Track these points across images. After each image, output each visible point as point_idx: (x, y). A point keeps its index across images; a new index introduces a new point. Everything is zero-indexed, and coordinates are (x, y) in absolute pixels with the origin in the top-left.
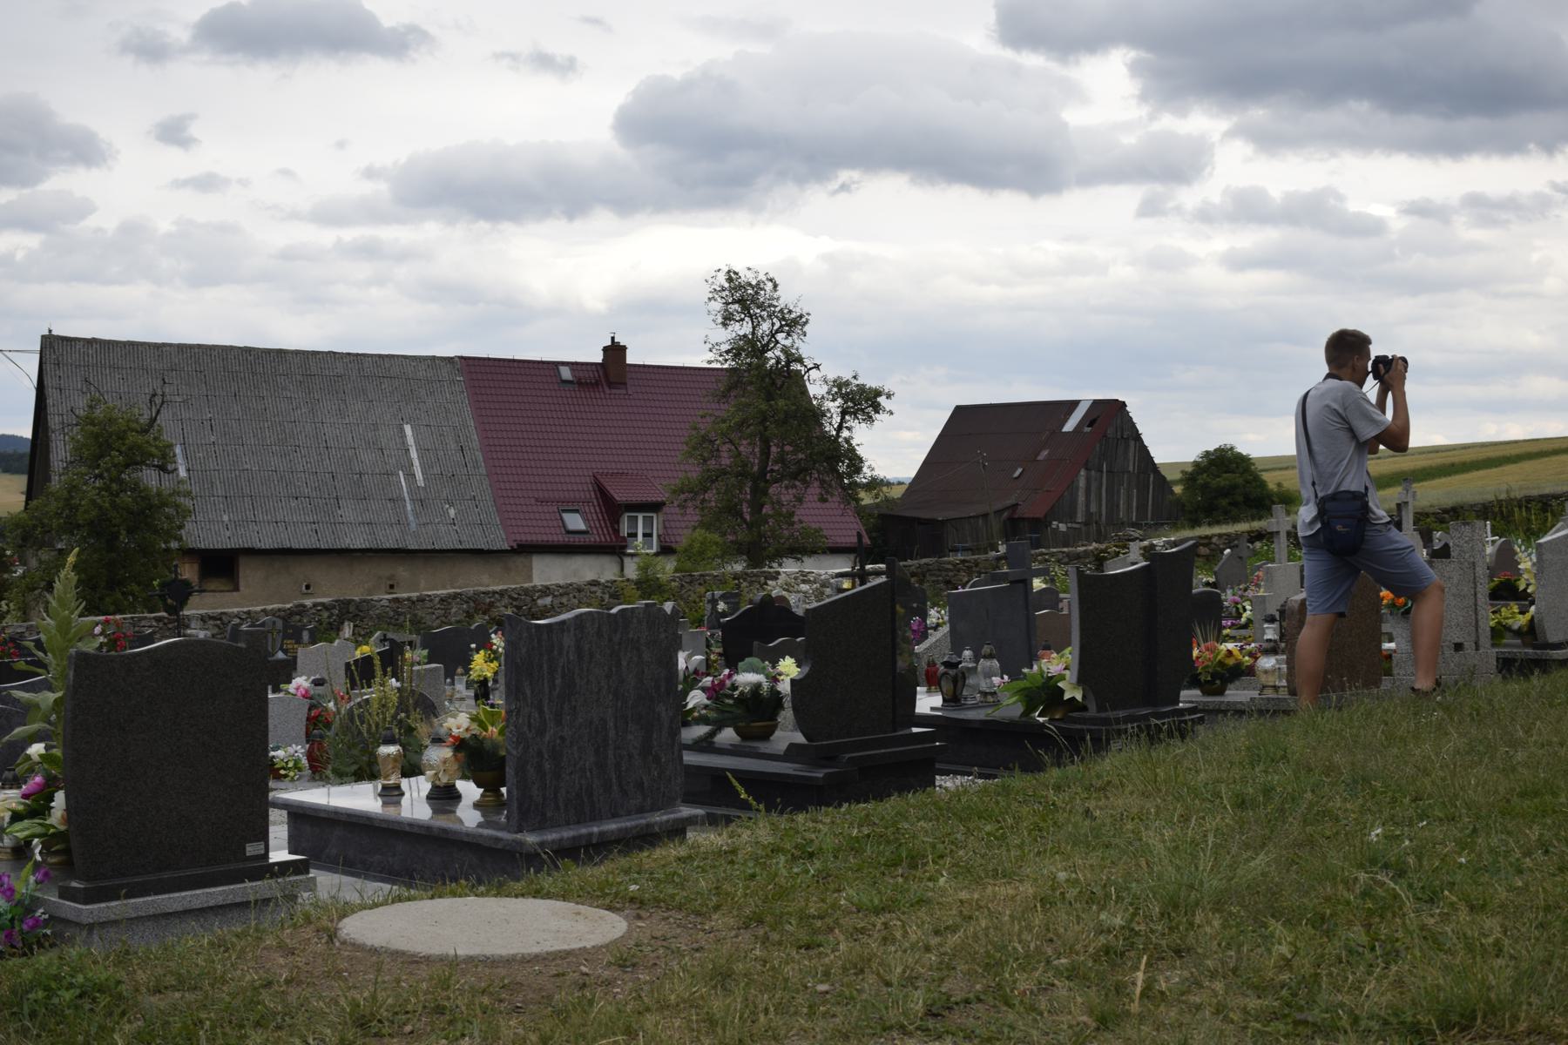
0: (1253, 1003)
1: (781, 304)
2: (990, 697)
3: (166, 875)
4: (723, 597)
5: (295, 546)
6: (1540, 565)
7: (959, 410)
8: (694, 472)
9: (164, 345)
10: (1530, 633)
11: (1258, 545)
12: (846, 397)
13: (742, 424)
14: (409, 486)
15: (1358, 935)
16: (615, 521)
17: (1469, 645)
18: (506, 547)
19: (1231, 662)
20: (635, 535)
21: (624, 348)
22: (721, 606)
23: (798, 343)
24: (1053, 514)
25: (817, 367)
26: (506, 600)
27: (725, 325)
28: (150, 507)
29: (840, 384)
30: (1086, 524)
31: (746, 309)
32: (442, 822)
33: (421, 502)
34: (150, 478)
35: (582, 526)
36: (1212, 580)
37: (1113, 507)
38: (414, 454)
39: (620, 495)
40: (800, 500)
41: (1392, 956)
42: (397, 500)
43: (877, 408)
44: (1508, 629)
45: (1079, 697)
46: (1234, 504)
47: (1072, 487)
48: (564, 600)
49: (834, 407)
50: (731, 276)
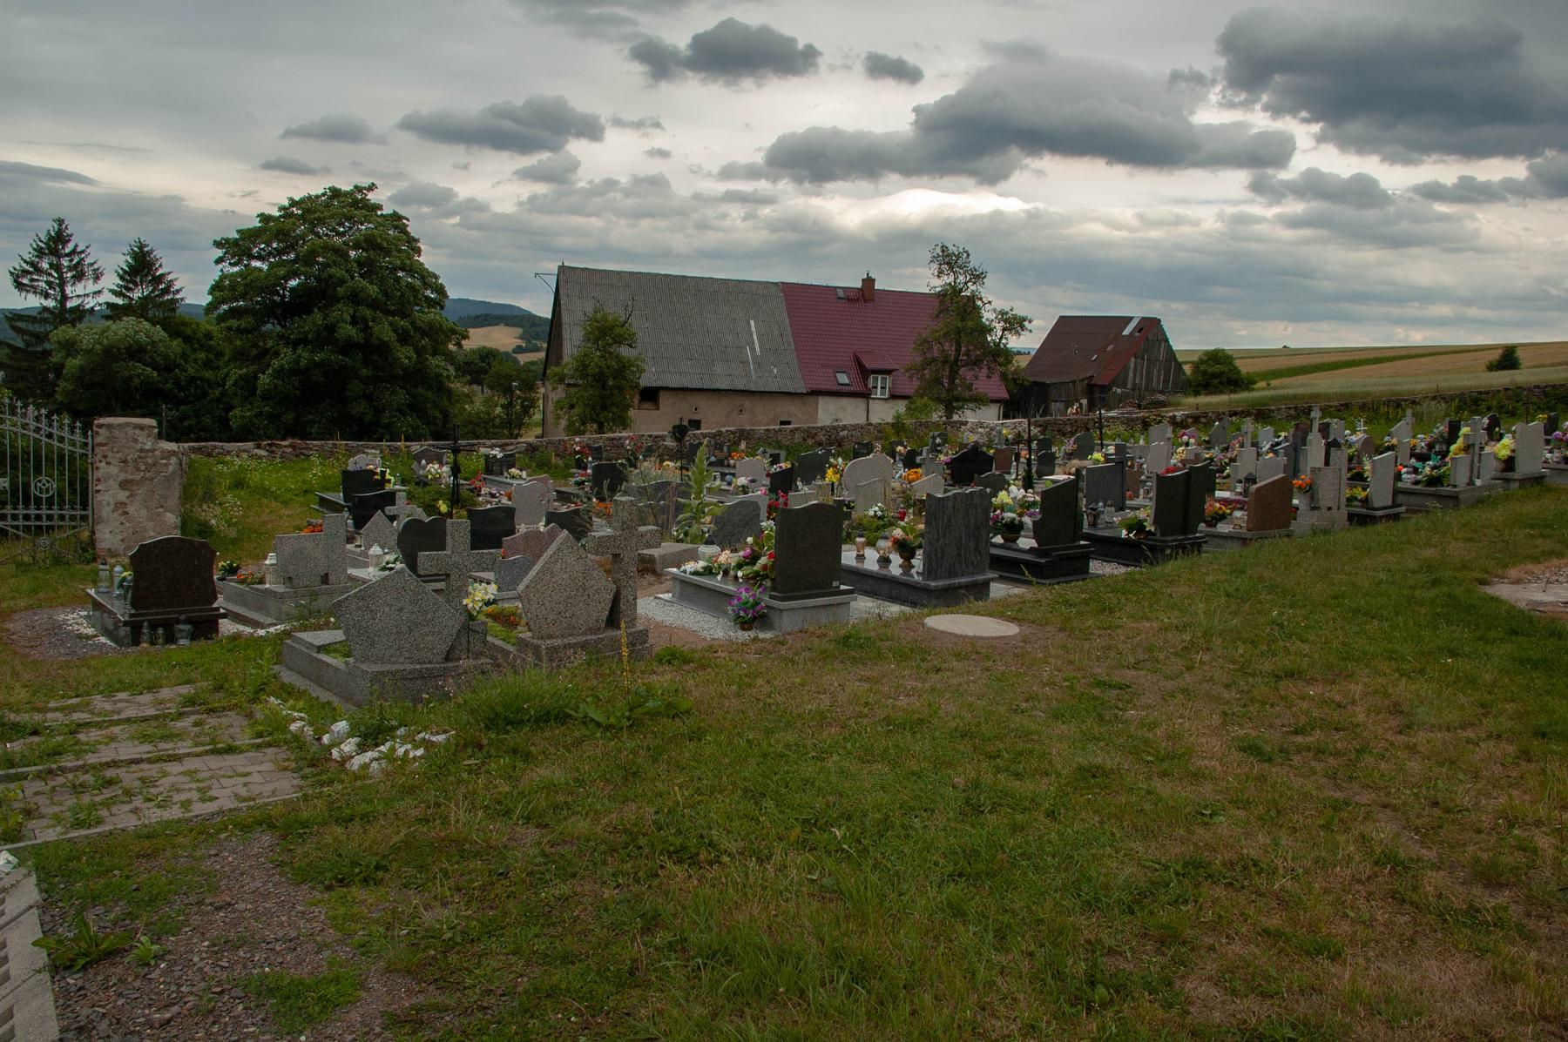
0: (1232, 667)
1: (971, 265)
2: (1110, 525)
3: (795, 594)
4: (939, 435)
5: (690, 386)
6: (1373, 467)
7: (1061, 317)
8: (919, 359)
9: (622, 272)
10: (1366, 502)
11: (1234, 418)
12: (1006, 321)
13: (945, 335)
14: (752, 354)
15: (1265, 647)
16: (865, 379)
17: (1335, 508)
18: (805, 391)
19: (1221, 512)
20: (876, 387)
21: (874, 280)
22: (938, 441)
23: (980, 289)
24: (1114, 383)
25: (990, 302)
26: (824, 432)
27: (939, 277)
28: (624, 367)
29: (1003, 313)
30: (1133, 390)
31: (951, 268)
32: (884, 572)
33: (758, 364)
34: (624, 351)
35: (847, 381)
36: (1207, 439)
37: (1149, 380)
38: (755, 337)
39: (869, 365)
40: (976, 378)
41: (1275, 655)
42: (746, 363)
43: (1023, 327)
44: (1356, 498)
45: (1153, 530)
46: (1221, 383)
47: (1126, 368)
48: (854, 433)
49: (999, 326)
50: (944, 249)
